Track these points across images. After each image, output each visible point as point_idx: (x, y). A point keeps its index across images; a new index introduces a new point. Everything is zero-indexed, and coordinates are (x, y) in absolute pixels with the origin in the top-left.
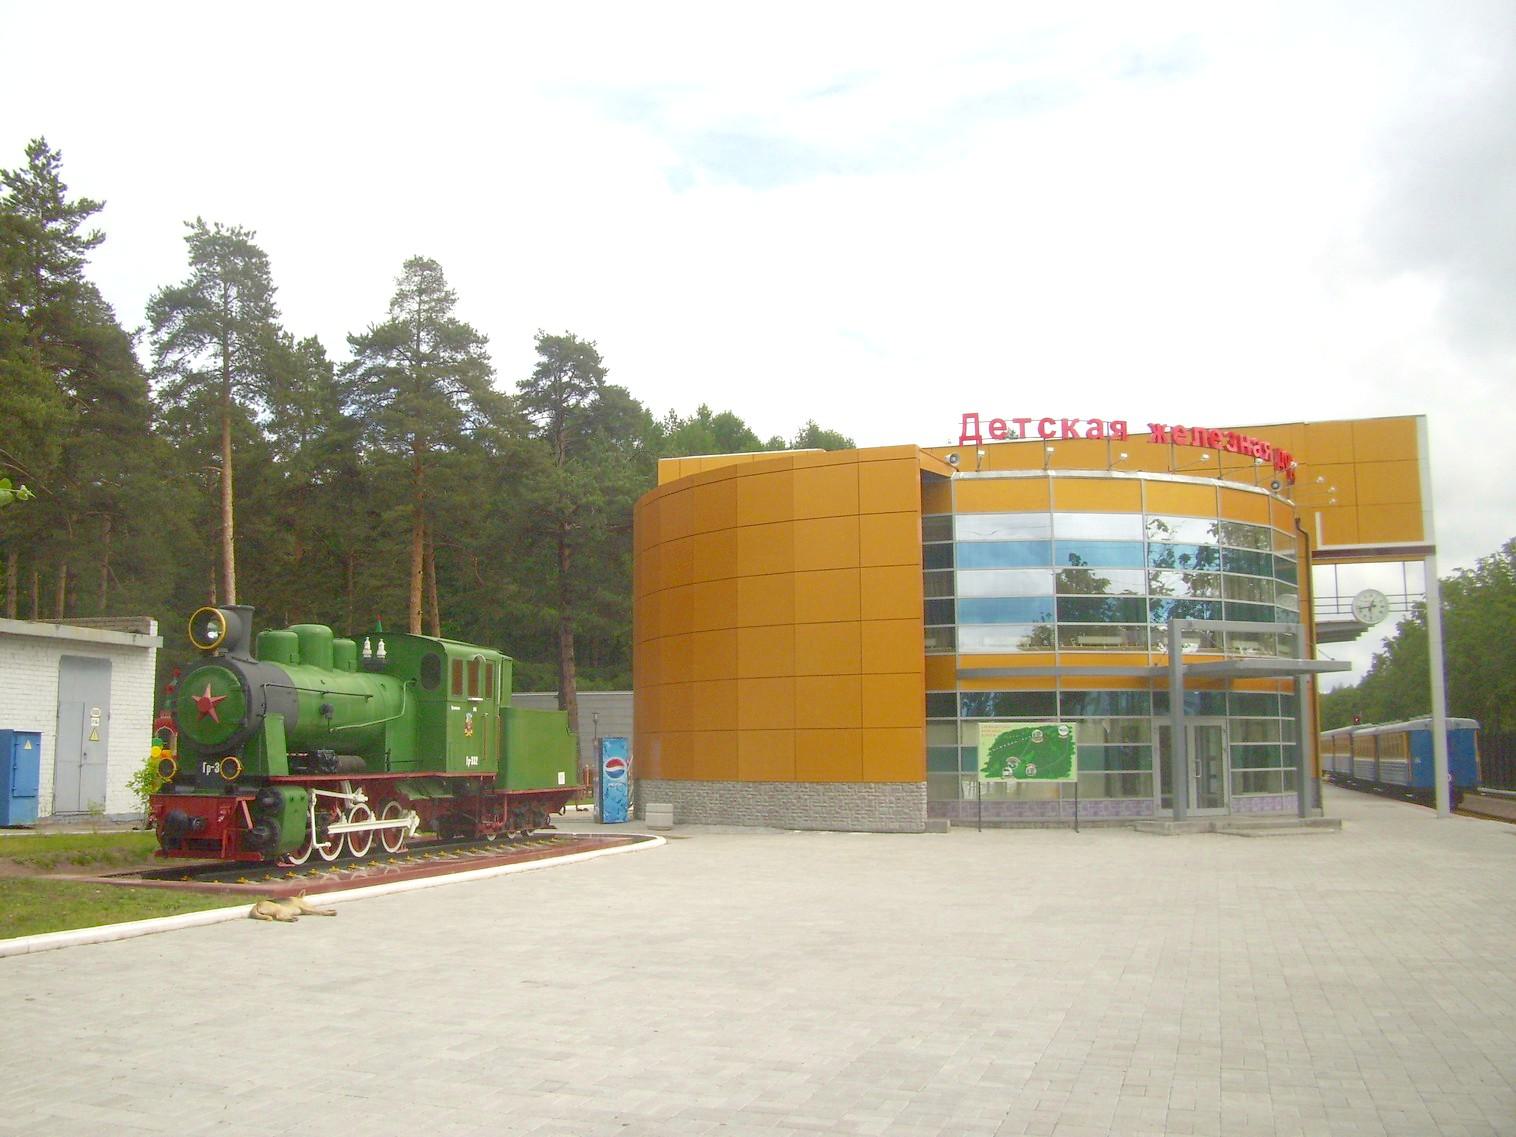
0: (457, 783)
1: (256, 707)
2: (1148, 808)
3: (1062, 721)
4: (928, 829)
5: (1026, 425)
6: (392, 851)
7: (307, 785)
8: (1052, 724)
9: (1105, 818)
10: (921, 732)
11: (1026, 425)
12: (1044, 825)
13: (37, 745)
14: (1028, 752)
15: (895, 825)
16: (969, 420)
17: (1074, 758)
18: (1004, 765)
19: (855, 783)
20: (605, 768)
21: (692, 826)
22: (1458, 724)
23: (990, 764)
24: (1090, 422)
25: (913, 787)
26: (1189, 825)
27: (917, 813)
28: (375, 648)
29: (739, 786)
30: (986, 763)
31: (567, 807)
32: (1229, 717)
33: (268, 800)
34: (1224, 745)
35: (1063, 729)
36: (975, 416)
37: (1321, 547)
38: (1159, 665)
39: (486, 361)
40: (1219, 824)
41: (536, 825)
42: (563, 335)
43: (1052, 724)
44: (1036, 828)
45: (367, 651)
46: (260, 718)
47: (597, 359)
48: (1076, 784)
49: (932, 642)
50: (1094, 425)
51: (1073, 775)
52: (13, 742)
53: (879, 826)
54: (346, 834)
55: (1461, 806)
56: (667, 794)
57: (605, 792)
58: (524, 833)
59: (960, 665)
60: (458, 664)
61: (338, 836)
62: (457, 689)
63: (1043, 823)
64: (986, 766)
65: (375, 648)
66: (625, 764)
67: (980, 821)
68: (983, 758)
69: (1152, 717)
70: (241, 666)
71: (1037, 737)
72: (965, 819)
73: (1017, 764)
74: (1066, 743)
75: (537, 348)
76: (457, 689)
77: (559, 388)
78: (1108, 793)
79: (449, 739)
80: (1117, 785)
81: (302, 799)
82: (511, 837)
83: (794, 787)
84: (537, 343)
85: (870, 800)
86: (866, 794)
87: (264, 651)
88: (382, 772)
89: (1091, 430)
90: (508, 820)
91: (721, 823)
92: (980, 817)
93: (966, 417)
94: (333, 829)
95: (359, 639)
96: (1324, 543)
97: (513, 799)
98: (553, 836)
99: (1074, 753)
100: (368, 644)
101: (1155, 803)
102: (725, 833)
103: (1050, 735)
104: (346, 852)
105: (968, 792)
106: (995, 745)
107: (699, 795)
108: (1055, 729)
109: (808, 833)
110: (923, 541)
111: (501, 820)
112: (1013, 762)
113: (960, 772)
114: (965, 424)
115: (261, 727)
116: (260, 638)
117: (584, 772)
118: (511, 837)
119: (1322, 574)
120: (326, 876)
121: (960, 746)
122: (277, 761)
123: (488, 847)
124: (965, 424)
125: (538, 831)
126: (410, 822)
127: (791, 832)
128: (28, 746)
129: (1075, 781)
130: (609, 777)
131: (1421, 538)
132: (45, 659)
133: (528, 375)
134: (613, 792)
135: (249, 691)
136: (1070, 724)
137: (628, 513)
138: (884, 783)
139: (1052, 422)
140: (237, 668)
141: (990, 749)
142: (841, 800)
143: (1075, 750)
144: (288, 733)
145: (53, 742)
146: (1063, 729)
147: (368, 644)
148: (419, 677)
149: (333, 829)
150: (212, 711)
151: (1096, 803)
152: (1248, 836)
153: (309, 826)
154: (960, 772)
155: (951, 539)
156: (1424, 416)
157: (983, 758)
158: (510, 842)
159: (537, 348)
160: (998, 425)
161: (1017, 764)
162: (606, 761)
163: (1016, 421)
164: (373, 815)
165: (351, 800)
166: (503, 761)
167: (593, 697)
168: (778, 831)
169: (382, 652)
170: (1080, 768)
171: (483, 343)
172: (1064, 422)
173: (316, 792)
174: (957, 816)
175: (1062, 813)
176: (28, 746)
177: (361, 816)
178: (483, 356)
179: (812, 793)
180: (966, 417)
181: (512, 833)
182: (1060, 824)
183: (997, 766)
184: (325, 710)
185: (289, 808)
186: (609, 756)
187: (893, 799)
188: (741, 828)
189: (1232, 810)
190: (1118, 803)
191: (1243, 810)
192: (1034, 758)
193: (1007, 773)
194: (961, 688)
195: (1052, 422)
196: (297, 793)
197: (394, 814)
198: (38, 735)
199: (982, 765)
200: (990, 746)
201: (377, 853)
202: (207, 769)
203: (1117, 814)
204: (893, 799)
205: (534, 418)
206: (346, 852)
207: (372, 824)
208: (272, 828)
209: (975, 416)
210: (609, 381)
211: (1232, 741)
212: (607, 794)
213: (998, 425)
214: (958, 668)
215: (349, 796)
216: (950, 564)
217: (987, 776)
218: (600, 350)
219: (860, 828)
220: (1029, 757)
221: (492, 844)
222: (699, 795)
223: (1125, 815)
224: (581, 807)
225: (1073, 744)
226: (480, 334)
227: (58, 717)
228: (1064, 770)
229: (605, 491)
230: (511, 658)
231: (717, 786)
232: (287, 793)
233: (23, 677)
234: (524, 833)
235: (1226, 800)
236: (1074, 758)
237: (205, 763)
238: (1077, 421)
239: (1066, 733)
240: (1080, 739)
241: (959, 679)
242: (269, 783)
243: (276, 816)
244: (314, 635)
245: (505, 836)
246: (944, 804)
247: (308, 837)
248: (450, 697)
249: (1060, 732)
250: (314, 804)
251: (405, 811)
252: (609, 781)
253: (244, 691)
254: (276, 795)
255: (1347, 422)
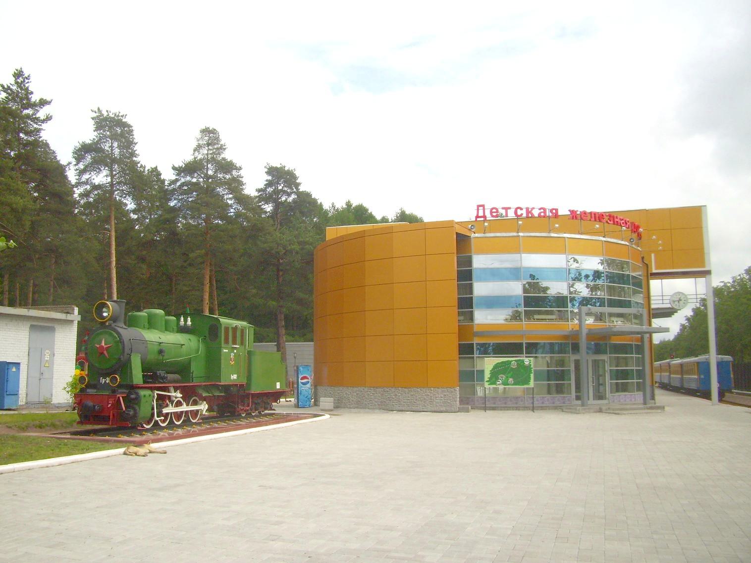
0: (226, 388)
1: (127, 350)
2: (569, 400)
3: (526, 357)
4: (460, 410)
5: (508, 210)
6: (194, 421)
7: (152, 389)
8: (521, 359)
9: (548, 405)
10: (456, 362)
11: (508, 210)
12: (517, 409)
13: (18, 369)
14: (509, 372)
15: (443, 409)
16: (480, 208)
17: (532, 376)
18: (497, 379)
19: (424, 388)
20: (300, 381)
21: (343, 409)
22: (722, 359)
23: (490, 378)
24: (540, 209)
25: (452, 390)
26: (589, 409)
27: (454, 402)
28: (186, 321)
29: (366, 389)
30: (488, 378)
31: (281, 400)
32: (609, 355)
33: (133, 396)
34: (606, 369)
35: (527, 361)
36: (483, 206)
37: (654, 271)
38: (574, 329)
39: (241, 179)
40: (604, 408)
41: (266, 409)
42: (279, 166)
43: (521, 359)
44: (513, 410)
45: (182, 323)
46: (129, 356)
47: (296, 178)
48: (533, 388)
49: (462, 318)
50: (542, 210)
51: (532, 384)
52: (6, 367)
53: (436, 409)
54: (171, 413)
55: (724, 399)
56: (330, 393)
57: (299, 392)
58: (260, 413)
59: (476, 329)
60: (227, 329)
61: (167, 414)
62: (227, 341)
63: (517, 407)
64: (488, 379)
65: (186, 321)
66: (310, 378)
67: (485, 407)
68: (487, 375)
69: (571, 355)
70: (119, 330)
71: (514, 365)
72: (478, 406)
73: (504, 379)
74: (528, 368)
75: (266, 172)
76: (227, 341)
77: (277, 192)
78: (549, 392)
79: (222, 366)
80: (554, 389)
81: (150, 395)
82: (253, 414)
83: (393, 390)
84: (266, 170)
85: (431, 396)
86: (429, 393)
87: (131, 322)
88: (189, 382)
89: (540, 213)
90: (252, 406)
91: (357, 408)
92: (485, 404)
93: (478, 206)
94: (165, 411)
95: (178, 316)
96: (656, 269)
97: (254, 396)
98: (274, 414)
99: (532, 373)
100: (182, 319)
101: (572, 397)
102: (359, 412)
103: (520, 364)
104: (171, 422)
105: (480, 392)
106: (493, 369)
107: (346, 394)
108: (523, 361)
109: (400, 412)
110: (457, 268)
111: (248, 406)
112: (502, 377)
113: (476, 382)
114: (478, 210)
115: (129, 360)
116: (129, 316)
117: (290, 382)
118: (253, 414)
119: (655, 284)
120: (162, 434)
121: (475, 369)
122: (137, 377)
123: (242, 420)
124: (478, 210)
125: (266, 412)
126: (203, 407)
127: (392, 412)
128: (14, 370)
129: (533, 386)
130: (302, 385)
131: (704, 267)
132: (22, 326)
133: (261, 185)
134: (304, 392)
135: (123, 342)
136: (530, 359)
137: (311, 254)
138: (438, 388)
139: (521, 209)
140: (117, 331)
141: (491, 371)
142: (416, 396)
143: (533, 372)
144: (143, 363)
145: (26, 368)
146: (527, 361)
147: (182, 319)
148: (207, 335)
149: (165, 411)
150: (105, 352)
151: (543, 397)
152: (618, 414)
153: (153, 409)
154: (476, 382)
155: (471, 267)
156: (705, 206)
157: (487, 375)
158: (253, 417)
159: (266, 172)
160: (494, 210)
161: (504, 379)
162: (300, 377)
163: (503, 208)
164: (185, 403)
165: (174, 396)
166: (249, 377)
167: (294, 345)
168: (386, 411)
169: (189, 323)
170: (535, 380)
171: (239, 170)
172: (527, 209)
173: (156, 392)
174: (474, 404)
175: (526, 403)
176: (14, 370)
177: (179, 404)
178: (239, 176)
179: (402, 393)
180: (478, 206)
181: (254, 413)
182: (525, 408)
183: (494, 379)
184: (161, 352)
185: (143, 400)
186: (302, 375)
187: (442, 396)
188: (367, 410)
189: (610, 401)
190: (554, 398)
191: (616, 401)
192: (512, 375)
193: (499, 383)
194: (476, 341)
195: (521, 209)
196: (147, 393)
197: (195, 403)
198: (19, 364)
199: (486, 379)
200: (491, 369)
201: (187, 422)
202: (102, 381)
203: (553, 403)
204: (442, 396)
205: (264, 207)
206: (171, 422)
207: (184, 408)
208: (135, 410)
209: (483, 206)
210: (302, 188)
211: (610, 367)
212: (301, 393)
213: (494, 210)
214: (474, 331)
215: (173, 394)
216: (471, 279)
217: (489, 384)
218: (297, 173)
219: (426, 410)
220: (510, 375)
221: (244, 418)
222: (346, 394)
223: (557, 403)
224: (288, 399)
225: (532, 368)
226: (238, 165)
227: (29, 355)
228: (527, 381)
229: (300, 243)
230: (253, 326)
231: (355, 389)
232: (142, 393)
233: (11, 335)
234: (260, 413)
235: (607, 396)
236: (532, 376)
237: (101, 378)
238: (533, 208)
239: (528, 363)
240: (535, 366)
241: (475, 336)
242: (133, 388)
243: (137, 404)
244: (156, 315)
245: (250, 414)
246: (468, 398)
247: (153, 415)
248: (223, 345)
249: (525, 363)
250: (156, 398)
251: (201, 402)
252: (302, 387)
253: (121, 342)
254: (137, 394)
255: (667, 209)
